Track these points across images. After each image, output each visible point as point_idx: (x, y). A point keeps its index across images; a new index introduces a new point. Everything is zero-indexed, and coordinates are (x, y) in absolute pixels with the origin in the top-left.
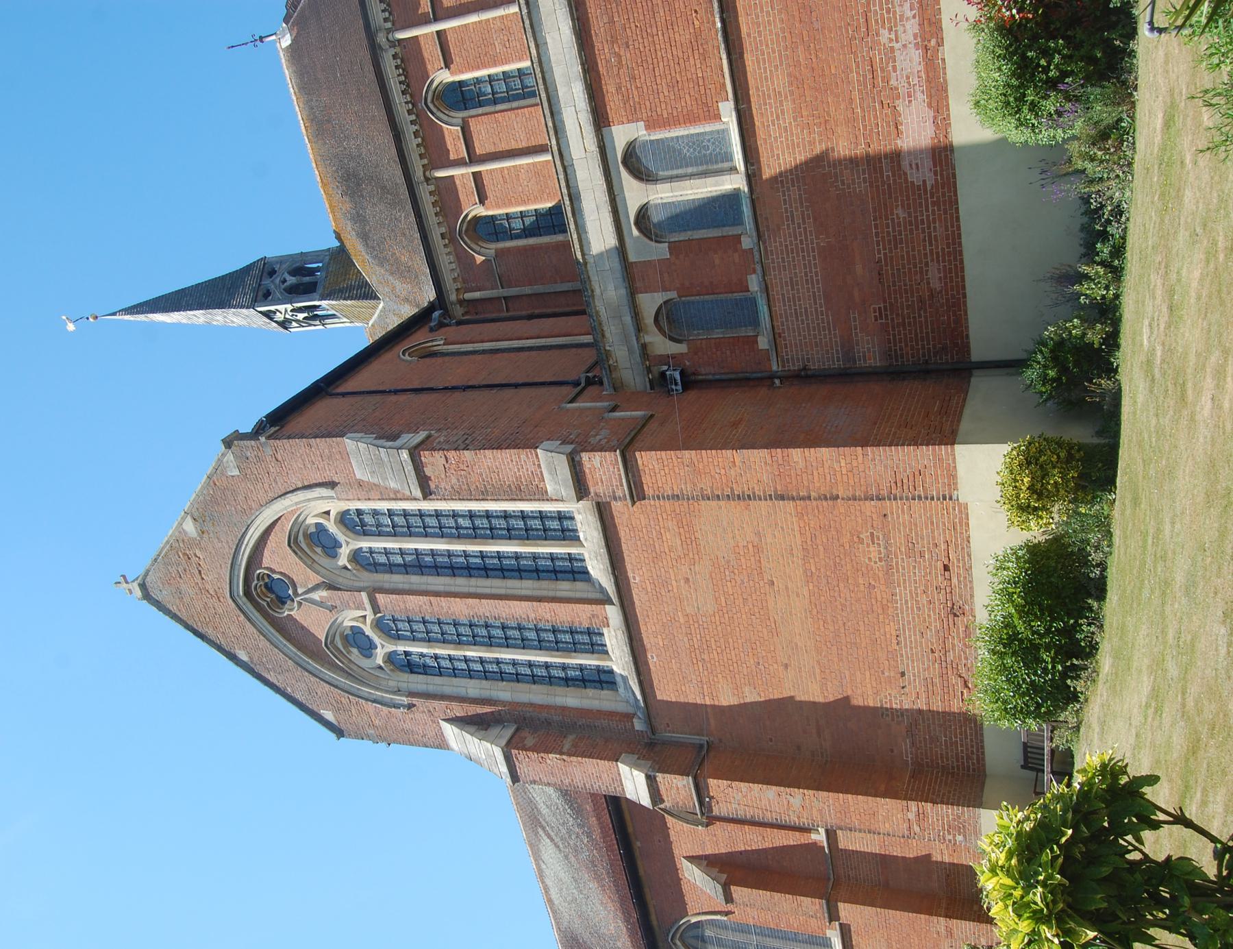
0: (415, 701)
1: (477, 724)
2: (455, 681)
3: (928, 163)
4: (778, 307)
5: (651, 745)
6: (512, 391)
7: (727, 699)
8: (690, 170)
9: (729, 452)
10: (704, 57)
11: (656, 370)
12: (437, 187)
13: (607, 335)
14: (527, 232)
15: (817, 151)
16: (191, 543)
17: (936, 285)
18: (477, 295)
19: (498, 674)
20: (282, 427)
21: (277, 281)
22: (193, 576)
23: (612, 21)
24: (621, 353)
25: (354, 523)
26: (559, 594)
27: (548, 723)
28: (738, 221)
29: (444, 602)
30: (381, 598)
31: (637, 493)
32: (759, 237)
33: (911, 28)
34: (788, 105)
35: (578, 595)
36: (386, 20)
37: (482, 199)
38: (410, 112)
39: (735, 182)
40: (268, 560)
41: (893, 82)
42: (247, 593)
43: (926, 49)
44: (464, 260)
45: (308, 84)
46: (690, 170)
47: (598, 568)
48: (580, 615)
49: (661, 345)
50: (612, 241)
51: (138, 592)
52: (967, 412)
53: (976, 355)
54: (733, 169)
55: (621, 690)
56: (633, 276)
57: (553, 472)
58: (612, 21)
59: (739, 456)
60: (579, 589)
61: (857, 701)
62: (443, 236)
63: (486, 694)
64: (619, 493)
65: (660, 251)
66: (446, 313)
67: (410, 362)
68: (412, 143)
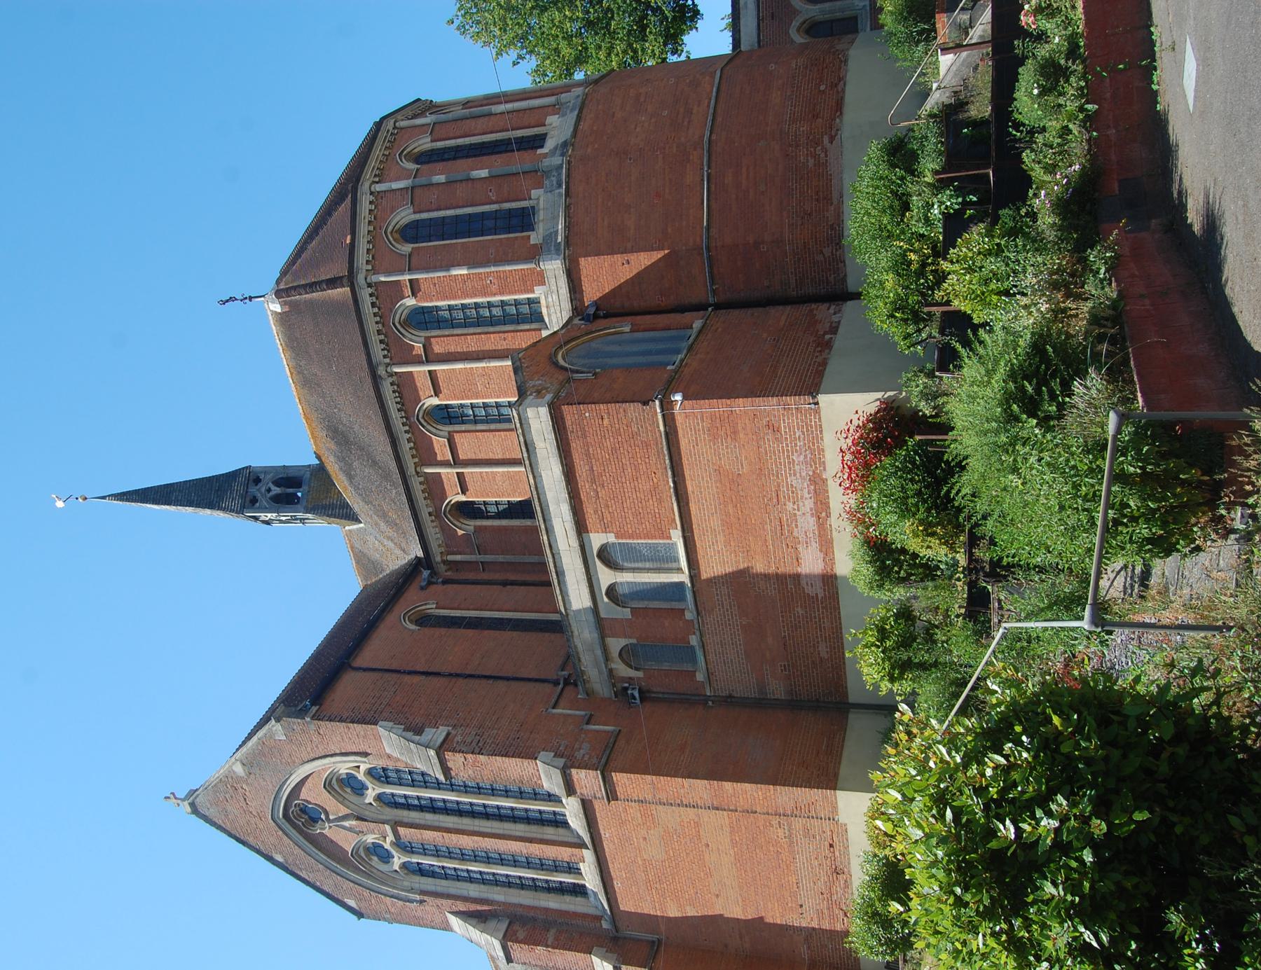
0: (426, 898)
1: (479, 917)
2: (459, 884)
3: (819, 584)
4: (711, 657)
5: (615, 939)
6: (506, 683)
7: (673, 912)
8: (648, 565)
9: (680, 780)
10: (660, 501)
11: (619, 685)
12: (426, 479)
13: (583, 660)
14: (499, 515)
15: (741, 567)
16: (239, 779)
17: (824, 655)
18: (458, 558)
19: (495, 882)
20: (321, 705)
21: (263, 490)
22: (238, 801)
23: (592, 469)
24: (590, 666)
25: (380, 775)
26: (546, 837)
27: (534, 919)
28: (682, 598)
29: (454, 837)
30: (401, 830)
31: (612, 795)
32: (698, 614)
33: (809, 504)
34: (721, 538)
35: (560, 839)
36: (385, 357)
37: (464, 490)
38: (404, 424)
39: (684, 578)
40: (305, 794)
41: (795, 534)
42: (286, 815)
44: (448, 533)
45: (295, 344)
46: (648, 565)
47: (576, 822)
48: (564, 854)
49: (623, 670)
50: (587, 603)
51: (189, 810)
52: (848, 743)
53: (852, 699)
54: (680, 570)
55: (592, 899)
56: (603, 626)
57: (550, 777)
58: (592, 469)
59: (687, 782)
60: (560, 834)
61: (769, 920)
62: (430, 514)
63: (484, 896)
64: (598, 795)
65: (626, 614)
66: (434, 573)
67: (413, 631)
68: (406, 447)
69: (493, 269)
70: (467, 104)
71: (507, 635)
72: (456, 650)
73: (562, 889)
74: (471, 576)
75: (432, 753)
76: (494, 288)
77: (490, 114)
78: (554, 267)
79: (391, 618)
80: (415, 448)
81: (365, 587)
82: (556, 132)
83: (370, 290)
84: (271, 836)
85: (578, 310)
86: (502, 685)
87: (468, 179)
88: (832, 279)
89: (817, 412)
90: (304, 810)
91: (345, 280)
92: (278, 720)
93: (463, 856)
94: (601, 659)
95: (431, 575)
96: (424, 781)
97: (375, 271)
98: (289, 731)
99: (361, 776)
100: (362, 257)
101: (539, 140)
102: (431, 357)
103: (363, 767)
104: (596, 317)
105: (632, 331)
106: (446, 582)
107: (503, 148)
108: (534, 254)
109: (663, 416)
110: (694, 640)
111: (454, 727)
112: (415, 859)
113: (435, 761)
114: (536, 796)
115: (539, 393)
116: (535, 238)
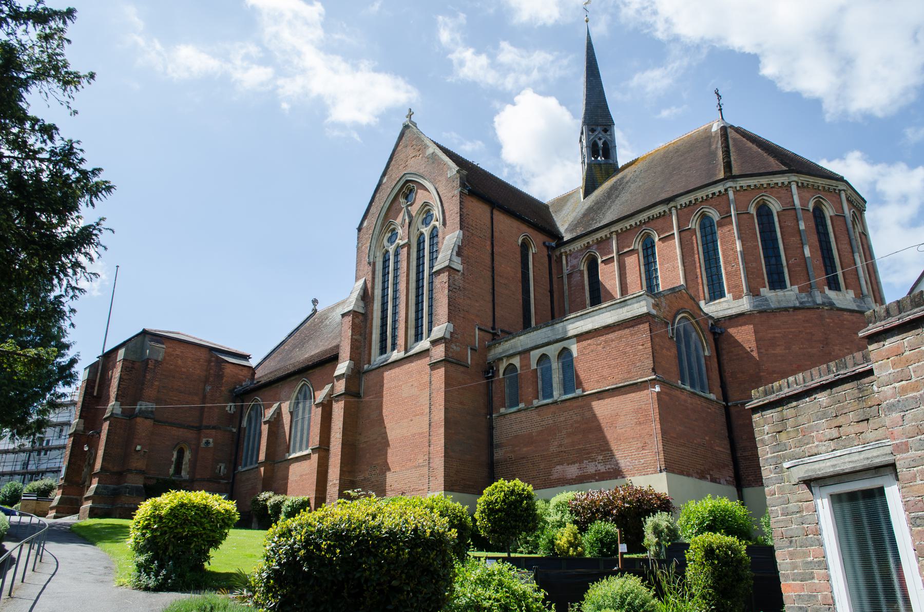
1: (366, 296)
4: (513, 416)
6: (491, 299)
10: (598, 382)
25: (434, 235)
28: (544, 398)
29: (405, 278)
30: (405, 249)
32: (537, 407)
42: (408, 181)
43: (595, 475)
48: (401, 341)
57: (439, 330)
59: (442, 407)
65: (534, 366)
69: (741, 267)
70: (864, 235)
71: (519, 296)
72: (509, 268)
73: (383, 340)
74: (554, 271)
75: (446, 263)
76: (729, 269)
77: (853, 252)
78: (745, 304)
79: (524, 227)
80: (627, 230)
81: (546, 207)
82: (841, 297)
83: (723, 191)
84: (396, 174)
85: (717, 321)
86: (489, 298)
87: (802, 244)
88: (750, 478)
89: (656, 472)
90: (411, 191)
91: (728, 174)
92: (458, 172)
93: (395, 284)
94: (507, 354)
95: (552, 247)
96: (432, 260)
97: (736, 192)
98: (451, 180)
99: (433, 223)
100: (744, 182)
101: (834, 284)
102: (683, 234)
103: (437, 224)
104: (714, 334)
105: (705, 357)
106: (550, 257)
107: (828, 264)
108: (754, 292)
109: (646, 381)
110: (522, 406)
111: (463, 274)
112: (392, 258)
113: (443, 266)
114: (431, 323)
115: (656, 306)
116: (765, 291)
